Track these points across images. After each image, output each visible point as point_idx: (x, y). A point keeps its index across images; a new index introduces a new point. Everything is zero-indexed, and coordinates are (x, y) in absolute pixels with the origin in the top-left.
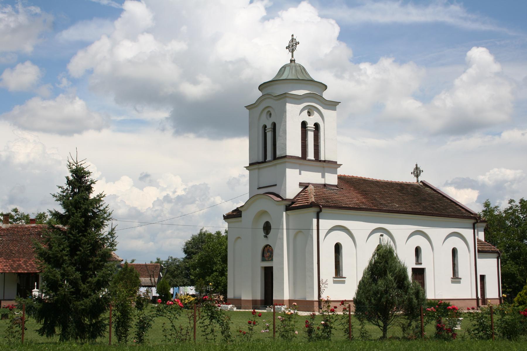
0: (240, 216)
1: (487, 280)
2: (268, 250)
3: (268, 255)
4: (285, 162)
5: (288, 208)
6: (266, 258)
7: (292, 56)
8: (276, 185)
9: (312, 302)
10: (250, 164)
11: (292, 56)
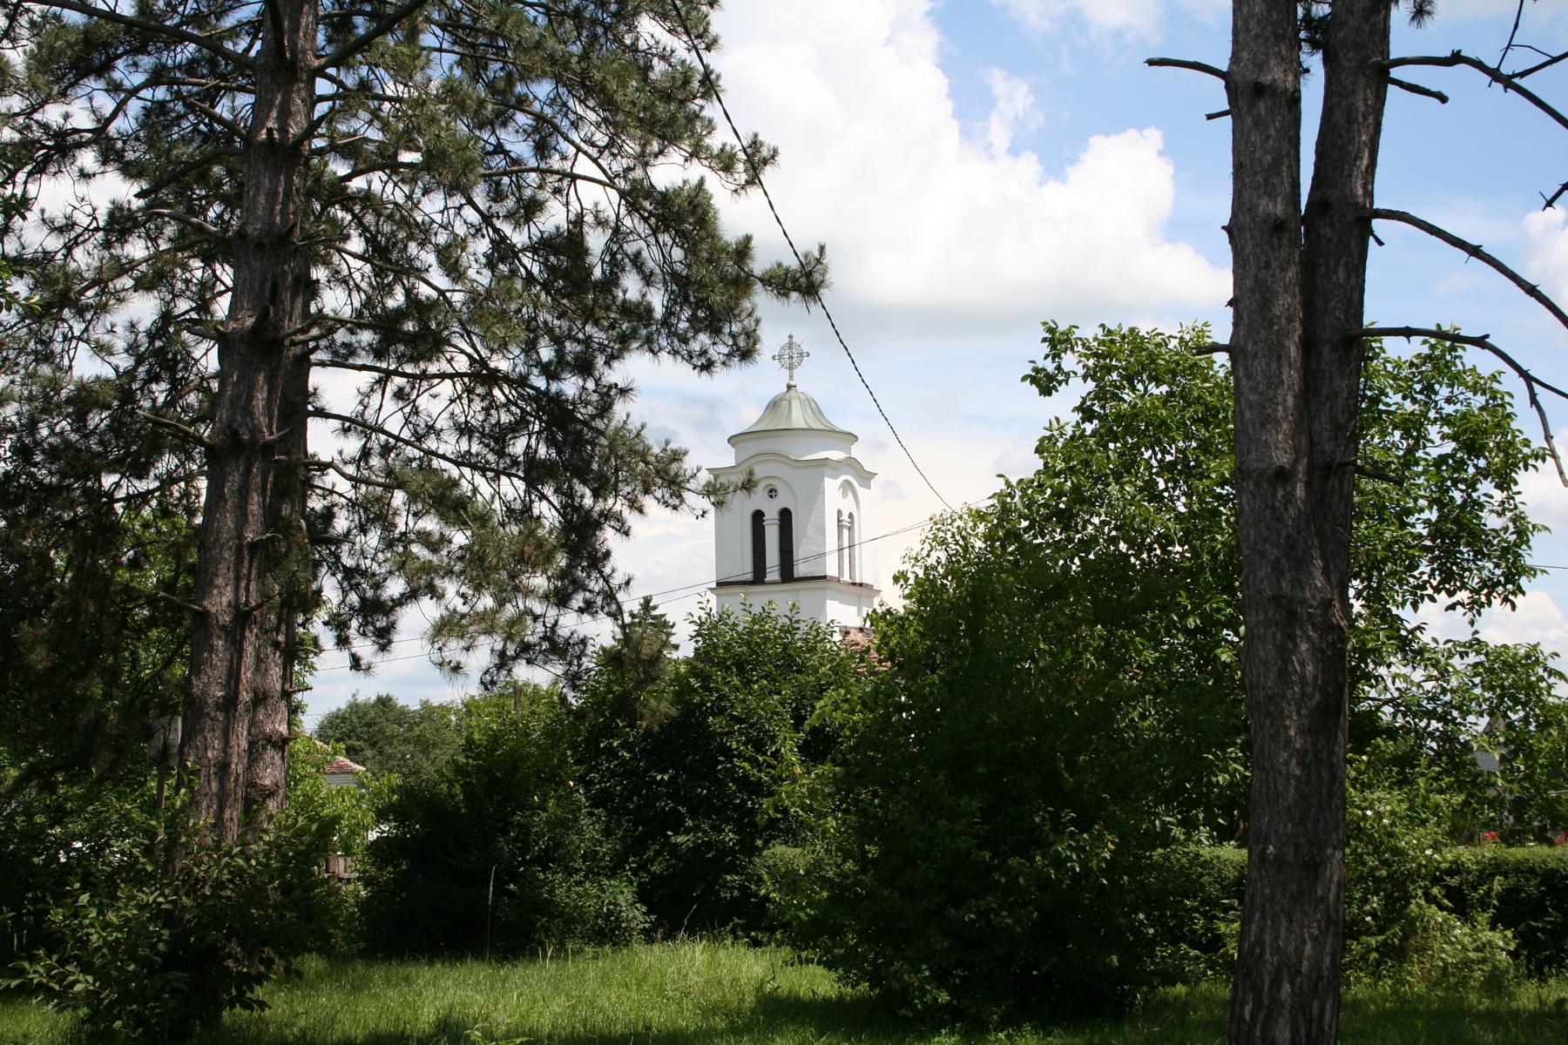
4: (824, 588)
7: (791, 377)
10: (720, 584)
11: (791, 377)
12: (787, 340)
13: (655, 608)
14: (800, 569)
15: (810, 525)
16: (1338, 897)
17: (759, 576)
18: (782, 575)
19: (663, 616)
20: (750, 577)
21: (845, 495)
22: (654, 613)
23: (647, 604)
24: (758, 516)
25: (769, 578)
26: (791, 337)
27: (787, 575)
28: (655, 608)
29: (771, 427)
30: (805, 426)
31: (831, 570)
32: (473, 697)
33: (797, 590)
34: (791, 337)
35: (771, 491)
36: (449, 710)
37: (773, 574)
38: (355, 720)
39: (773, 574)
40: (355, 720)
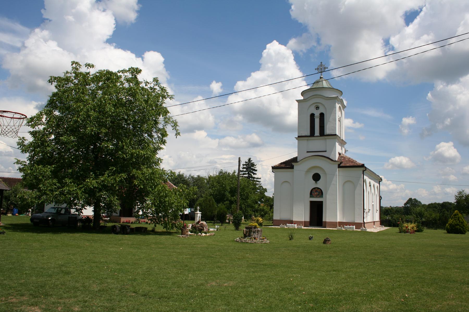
0: (292, 167)
1: (376, 211)
2: (316, 191)
3: (316, 194)
4: (335, 138)
5: (339, 167)
6: (314, 196)
8: (326, 151)
9: (362, 223)
10: (299, 137)
12: (320, 64)
13: (252, 161)
14: (327, 131)
15: (331, 118)
16: (453, 217)
17: (312, 134)
18: (320, 134)
19: (253, 163)
20: (309, 134)
21: (339, 111)
22: (251, 162)
23: (51, 204)
24: (312, 116)
25: (315, 135)
26: (321, 63)
27: (322, 133)
28: (252, 161)
29: (317, 87)
30: (327, 87)
31: (337, 133)
32: (211, 176)
33: (326, 139)
34: (321, 63)
35: (317, 108)
36: (204, 179)
37: (317, 132)
38: (179, 179)
39: (317, 132)
40: (179, 179)
